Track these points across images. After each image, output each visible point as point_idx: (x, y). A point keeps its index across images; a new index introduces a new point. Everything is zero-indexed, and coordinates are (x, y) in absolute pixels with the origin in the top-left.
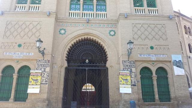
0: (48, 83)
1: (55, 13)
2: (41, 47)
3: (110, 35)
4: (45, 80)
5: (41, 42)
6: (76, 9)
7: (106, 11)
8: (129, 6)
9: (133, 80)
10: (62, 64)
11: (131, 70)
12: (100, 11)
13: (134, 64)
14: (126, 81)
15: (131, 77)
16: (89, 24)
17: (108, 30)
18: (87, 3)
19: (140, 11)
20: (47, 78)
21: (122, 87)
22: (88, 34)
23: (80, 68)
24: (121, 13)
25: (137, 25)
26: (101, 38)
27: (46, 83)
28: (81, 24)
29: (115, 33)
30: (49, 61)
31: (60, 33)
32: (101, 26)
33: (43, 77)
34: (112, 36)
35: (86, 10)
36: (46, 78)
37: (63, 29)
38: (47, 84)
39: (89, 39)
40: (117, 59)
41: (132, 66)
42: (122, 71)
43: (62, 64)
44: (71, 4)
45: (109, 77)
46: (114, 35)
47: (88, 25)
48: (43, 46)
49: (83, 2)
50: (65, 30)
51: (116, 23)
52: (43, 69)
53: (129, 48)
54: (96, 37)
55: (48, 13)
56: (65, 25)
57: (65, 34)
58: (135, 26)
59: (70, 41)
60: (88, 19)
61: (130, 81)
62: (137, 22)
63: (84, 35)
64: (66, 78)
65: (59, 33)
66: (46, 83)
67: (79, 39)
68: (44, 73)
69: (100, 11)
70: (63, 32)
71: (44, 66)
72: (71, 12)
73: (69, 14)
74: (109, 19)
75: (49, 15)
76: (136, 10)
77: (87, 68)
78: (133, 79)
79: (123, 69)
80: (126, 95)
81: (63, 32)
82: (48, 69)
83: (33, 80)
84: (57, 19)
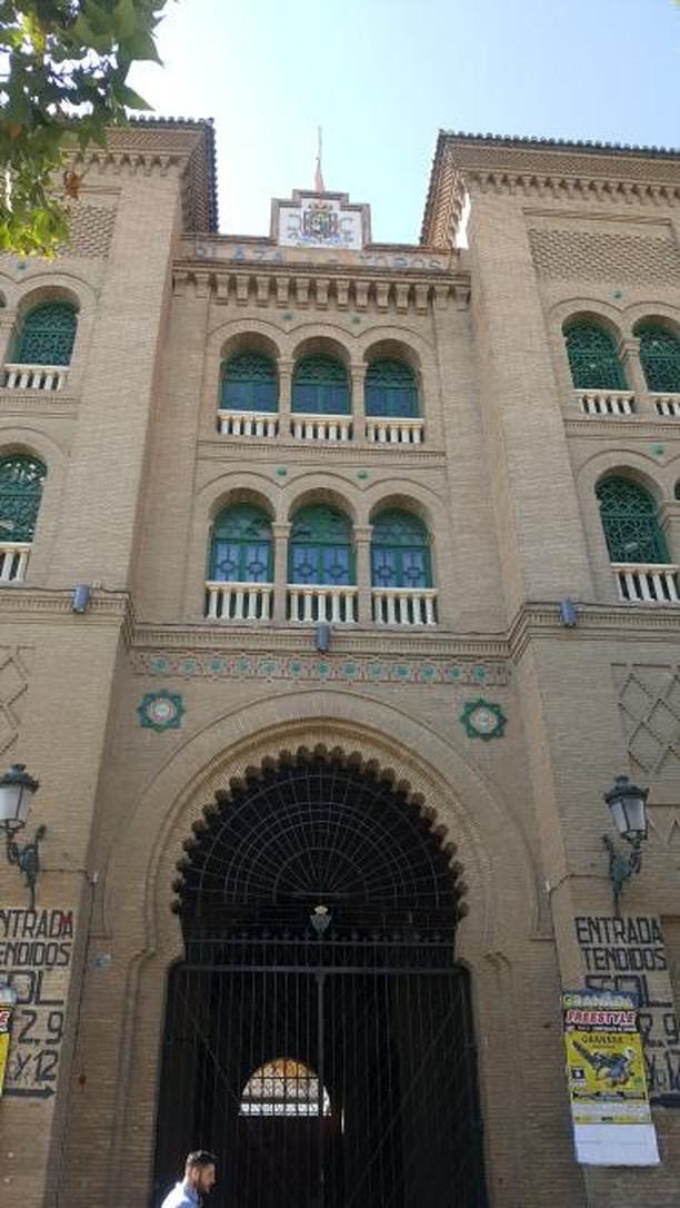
0: (53, 1085)
1: (120, 596)
2: (23, 825)
3: (473, 732)
4: (33, 1064)
5: (27, 792)
6: (378, 572)
7: (429, 584)
8: (580, 558)
9: (661, 1064)
10: (147, 943)
11: (641, 983)
12: (393, 580)
13: (659, 944)
14: (616, 1070)
15: (646, 1041)
16: (329, 663)
17: (454, 699)
18: (314, 538)
19: (652, 588)
20: (51, 1047)
21: (588, 1120)
22: (322, 725)
23: (275, 969)
24: (538, 599)
25: (641, 674)
26: (414, 753)
27: (44, 1084)
28: (278, 663)
29: (502, 721)
30: (66, 920)
31: (148, 723)
32: (409, 676)
33: (22, 1040)
34: (486, 737)
35: (227, 575)
36: (43, 1046)
37: (164, 694)
38: (47, 1092)
39: (329, 759)
40: (532, 904)
41: (643, 958)
42: (582, 994)
43: (153, 941)
44: (215, 541)
45: (484, 1043)
46: (498, 733)
47: (323, 669)
48: (40, 809)
49: (292, 532)
50: (175, 699)
51: (502, 659)
52: (23, 981)
53: (623, 828)
54: (377, 744)
55: (78, 596)
56: (181, 669)
57: (174, 723)
58: (630, 677)
59: (206, 773)
60: (327, 629)
61: (640, 1071)
62: (645, 652)
63: (300, 733)
64: (170, 1043)
65: (137, 719)
66: (44, 1084)
67: (266, 761)
68: (32, 1007)
69: (393, 580)
70: (162, 710)
71: (31, 959)
72: (214, 585)
73: (201, 600)
74: (457, 629)
75: (85, 605)
76: (623, 579)
77: (321, 972)
78: (662, 1051)
79: (588, 978)
80: (618, 1181)
81: (162, 710)
82: (57, 983)
83: (592, 1060)
84: (130, 632)
